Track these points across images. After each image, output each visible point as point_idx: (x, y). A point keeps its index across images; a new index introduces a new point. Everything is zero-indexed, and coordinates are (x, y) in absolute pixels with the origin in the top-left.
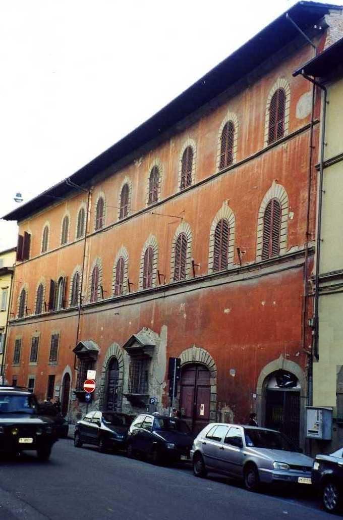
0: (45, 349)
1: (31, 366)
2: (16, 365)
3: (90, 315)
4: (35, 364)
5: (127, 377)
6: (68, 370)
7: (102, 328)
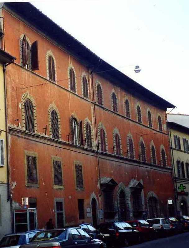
0: (69, 174)
1: (56, 189)
2: (33, 185)
3: (102, 159)
4: (61, 187)
5: (130, 203)
6: (93, 195)
7: (112, 171)
